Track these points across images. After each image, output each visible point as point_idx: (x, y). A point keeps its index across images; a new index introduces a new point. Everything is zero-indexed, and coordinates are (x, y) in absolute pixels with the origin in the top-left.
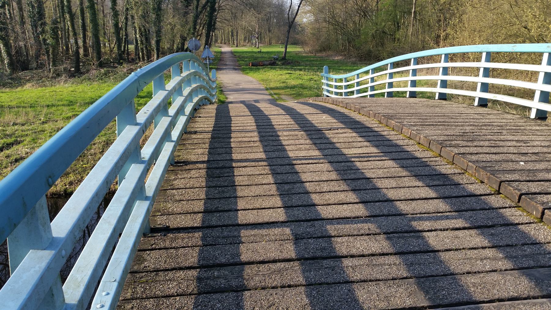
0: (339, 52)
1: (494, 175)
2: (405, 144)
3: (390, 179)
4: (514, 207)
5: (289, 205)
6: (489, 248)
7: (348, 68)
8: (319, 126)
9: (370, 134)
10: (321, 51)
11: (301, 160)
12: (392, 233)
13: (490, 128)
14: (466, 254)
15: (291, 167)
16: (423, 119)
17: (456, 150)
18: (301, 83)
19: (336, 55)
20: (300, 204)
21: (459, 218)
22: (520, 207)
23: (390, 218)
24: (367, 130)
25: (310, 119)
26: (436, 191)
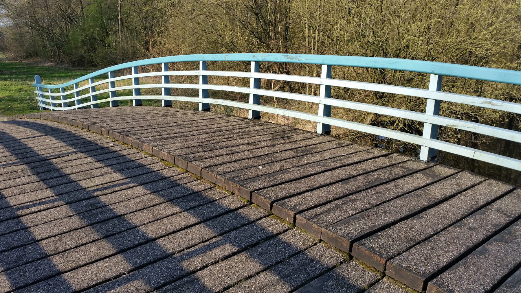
0: (48, 58)
1: (243, 185)
2: (149, 163)
3: (145, 211)
4: (268, 216)
5: (22, 283)
6: (263, 271)
7: (62, 75)
8: (45, 154)
9: (108, 156)
10: (27, 57)
11: (27, 207)
12: (164, 285)
13: (221, 133)
14: (245, 287)
15: (15, 221)
16: (160, 132)
17: (201, 164)
18: (8, 94)
19: (45, 62)
20: (39, 277)
21: (225, 244)
22: (273, 214)
23: (157, 264)
24: (103, 151)
25: (30, 146)
26: (195, 214)
